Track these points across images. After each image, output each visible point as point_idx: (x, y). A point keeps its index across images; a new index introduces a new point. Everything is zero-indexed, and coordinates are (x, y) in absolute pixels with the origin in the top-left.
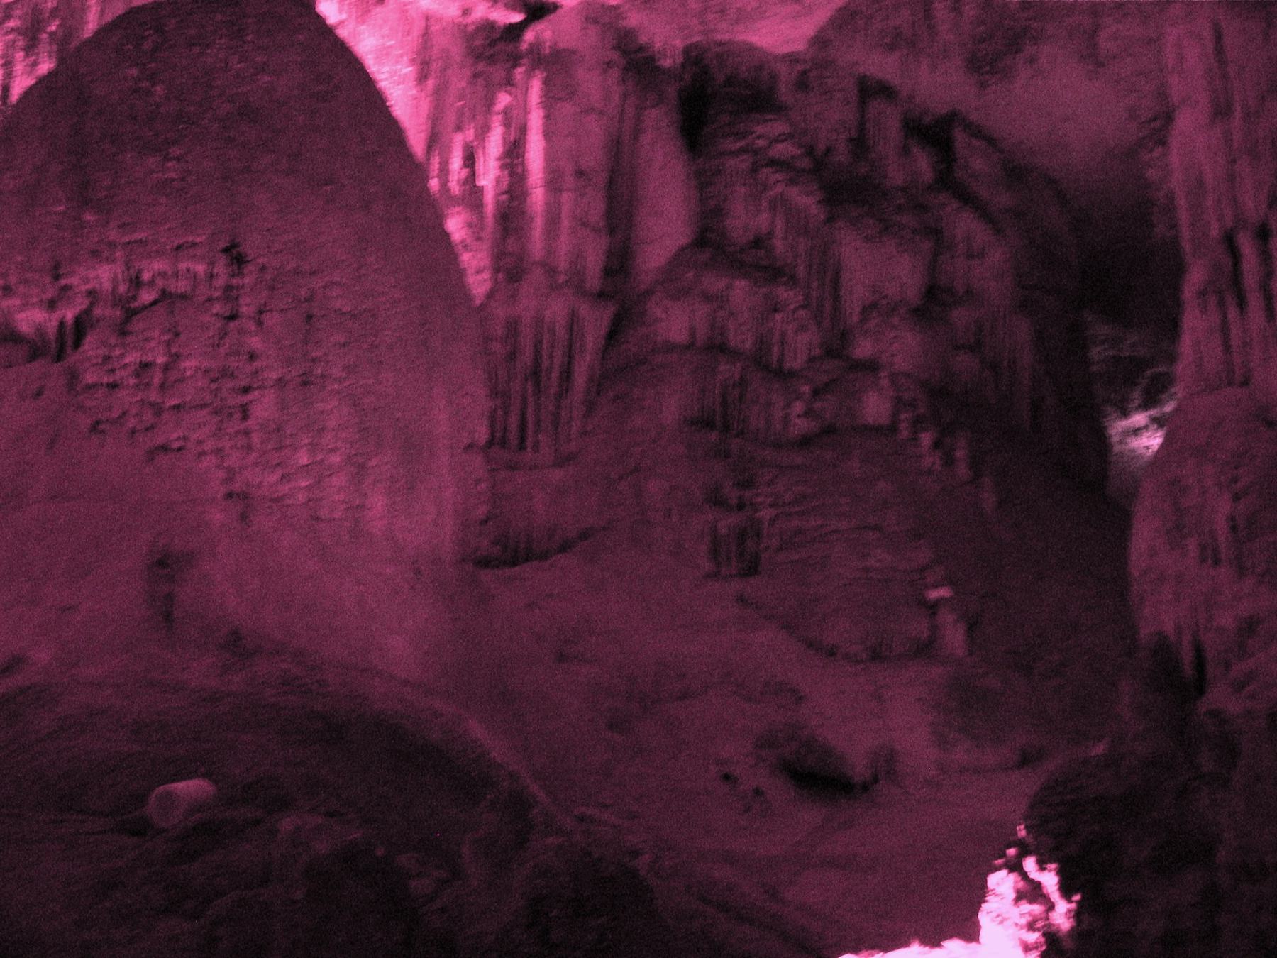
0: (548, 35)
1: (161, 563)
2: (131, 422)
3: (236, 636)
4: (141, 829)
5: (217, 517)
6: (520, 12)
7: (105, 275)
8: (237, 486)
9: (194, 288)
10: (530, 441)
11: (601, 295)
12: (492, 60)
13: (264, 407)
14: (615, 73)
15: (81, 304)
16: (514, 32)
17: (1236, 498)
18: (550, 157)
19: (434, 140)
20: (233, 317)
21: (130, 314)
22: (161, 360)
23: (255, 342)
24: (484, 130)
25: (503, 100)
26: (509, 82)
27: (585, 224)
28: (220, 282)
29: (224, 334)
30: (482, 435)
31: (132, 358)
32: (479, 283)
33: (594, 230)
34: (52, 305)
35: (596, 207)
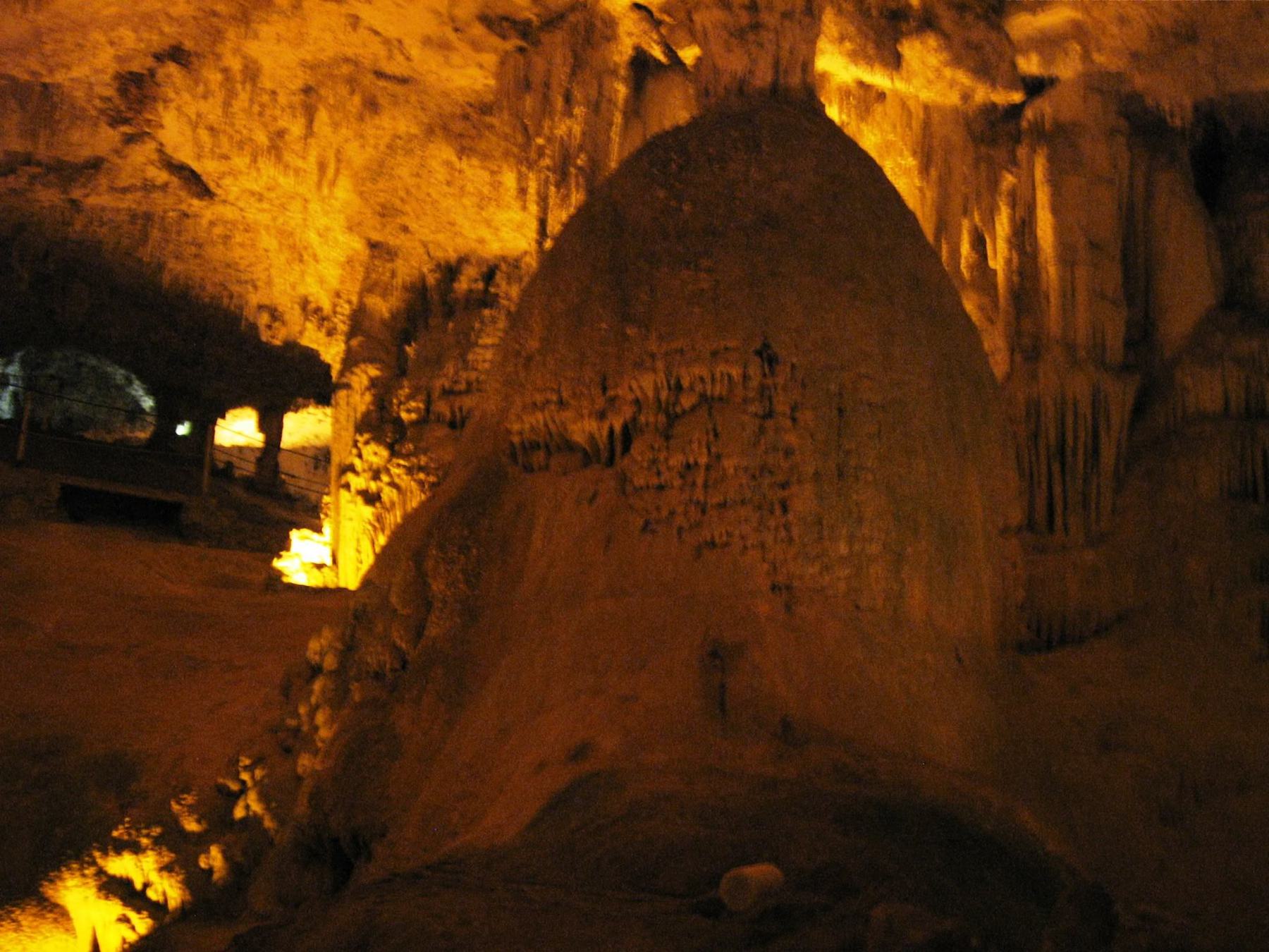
0: (1048, 110)
1: (714, 654)
2: (680, 520)
3: (786, 725)
4: (714, 910)
5: (763, 608)
6: (1017, 90)
7: (648, 383)
8: (781, 579)
9: (731, 391)
10: (1059, 521)
11: (1125, 369)
12: (993, 142)
13: (804, 500)
14: (1121, 139)
15: (628, 412)
16: (1015, 111)
17: (425, 214)
18: (1061, 230)
19: (943, 226)
20: (769, 415)
21: (673, 419)
22: (703, 460)
23: (792, 438)
24: (990, 216)
25: (1008, 180)
26: (1014, 162)
27: (1103, 296)
28: (754, 383)
29: (762, 430)
30: (1016, 516)
31: (676, 460)
32: (999, 365)
33: (1114, 303)
34: (602, 416)
35: (1113, 276)
